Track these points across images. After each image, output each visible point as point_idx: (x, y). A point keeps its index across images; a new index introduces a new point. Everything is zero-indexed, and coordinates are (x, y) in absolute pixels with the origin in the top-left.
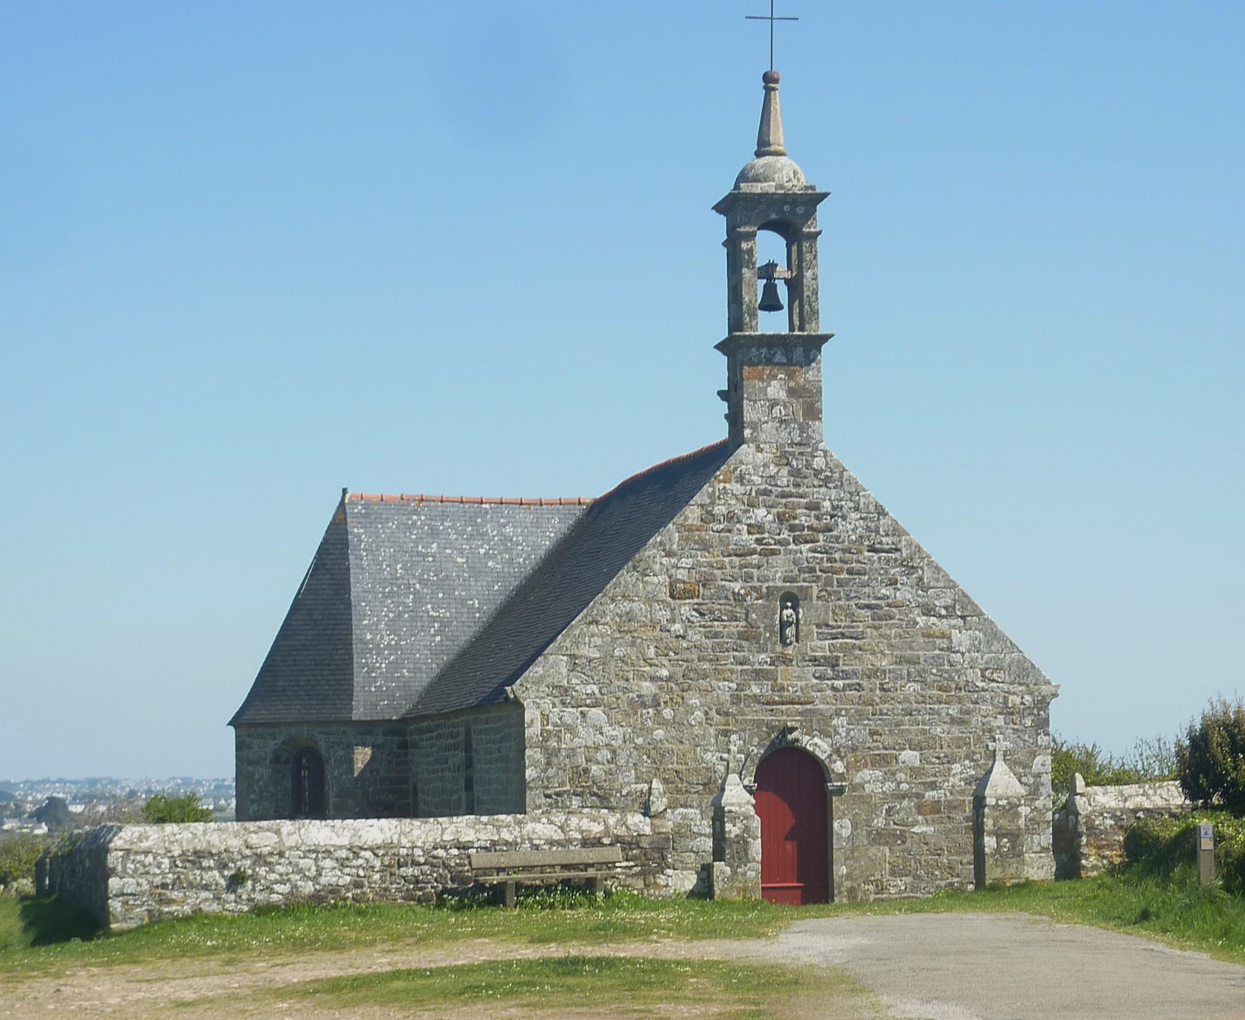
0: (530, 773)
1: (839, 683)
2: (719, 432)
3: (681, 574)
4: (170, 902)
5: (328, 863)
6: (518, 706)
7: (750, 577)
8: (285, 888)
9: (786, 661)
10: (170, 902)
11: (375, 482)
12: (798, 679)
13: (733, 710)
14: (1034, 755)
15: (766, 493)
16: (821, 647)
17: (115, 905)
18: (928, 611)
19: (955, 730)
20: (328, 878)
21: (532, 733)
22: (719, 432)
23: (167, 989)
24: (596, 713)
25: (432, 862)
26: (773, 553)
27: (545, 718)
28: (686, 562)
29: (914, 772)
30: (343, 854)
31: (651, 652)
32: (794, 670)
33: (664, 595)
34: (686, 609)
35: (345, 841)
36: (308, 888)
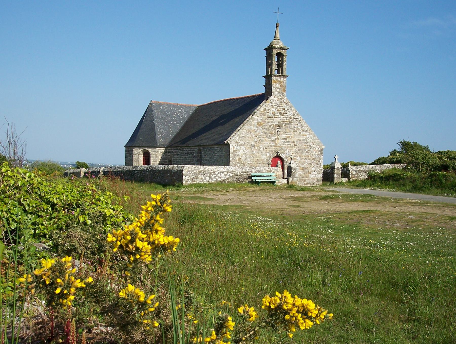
0: (231, 159)
1: (287, 144)
2: (263, 91)
3: (260, 121)
4: (194, 181)
5: (223, 175)
6: (228, 145)
7: (272, 122)
8: (215, 179)
9: (278, 139)
10: (194, 181)
11: (157, 99)
12: (280, 142)
13: (268, 148)
14: (320, 159)
15: (276, 106)
16: (284, 136)
17: (184, 182)
18: (303, 131)
19: (307, 154)
20: (223, 178)
21: (231, 151)
22: (263, 91)
23: (398, 209)
24: (243, 147)
25: (241, 175)
26: (276, 117)
27: (234, 148)
28: (261, 118)
29: (300, 162)
30: (225, 173)
31: (254, 136)
32: (280, 140)
33: (256, 125)
34: (260, 128)
35: (225, 170)
36: (219, 179)
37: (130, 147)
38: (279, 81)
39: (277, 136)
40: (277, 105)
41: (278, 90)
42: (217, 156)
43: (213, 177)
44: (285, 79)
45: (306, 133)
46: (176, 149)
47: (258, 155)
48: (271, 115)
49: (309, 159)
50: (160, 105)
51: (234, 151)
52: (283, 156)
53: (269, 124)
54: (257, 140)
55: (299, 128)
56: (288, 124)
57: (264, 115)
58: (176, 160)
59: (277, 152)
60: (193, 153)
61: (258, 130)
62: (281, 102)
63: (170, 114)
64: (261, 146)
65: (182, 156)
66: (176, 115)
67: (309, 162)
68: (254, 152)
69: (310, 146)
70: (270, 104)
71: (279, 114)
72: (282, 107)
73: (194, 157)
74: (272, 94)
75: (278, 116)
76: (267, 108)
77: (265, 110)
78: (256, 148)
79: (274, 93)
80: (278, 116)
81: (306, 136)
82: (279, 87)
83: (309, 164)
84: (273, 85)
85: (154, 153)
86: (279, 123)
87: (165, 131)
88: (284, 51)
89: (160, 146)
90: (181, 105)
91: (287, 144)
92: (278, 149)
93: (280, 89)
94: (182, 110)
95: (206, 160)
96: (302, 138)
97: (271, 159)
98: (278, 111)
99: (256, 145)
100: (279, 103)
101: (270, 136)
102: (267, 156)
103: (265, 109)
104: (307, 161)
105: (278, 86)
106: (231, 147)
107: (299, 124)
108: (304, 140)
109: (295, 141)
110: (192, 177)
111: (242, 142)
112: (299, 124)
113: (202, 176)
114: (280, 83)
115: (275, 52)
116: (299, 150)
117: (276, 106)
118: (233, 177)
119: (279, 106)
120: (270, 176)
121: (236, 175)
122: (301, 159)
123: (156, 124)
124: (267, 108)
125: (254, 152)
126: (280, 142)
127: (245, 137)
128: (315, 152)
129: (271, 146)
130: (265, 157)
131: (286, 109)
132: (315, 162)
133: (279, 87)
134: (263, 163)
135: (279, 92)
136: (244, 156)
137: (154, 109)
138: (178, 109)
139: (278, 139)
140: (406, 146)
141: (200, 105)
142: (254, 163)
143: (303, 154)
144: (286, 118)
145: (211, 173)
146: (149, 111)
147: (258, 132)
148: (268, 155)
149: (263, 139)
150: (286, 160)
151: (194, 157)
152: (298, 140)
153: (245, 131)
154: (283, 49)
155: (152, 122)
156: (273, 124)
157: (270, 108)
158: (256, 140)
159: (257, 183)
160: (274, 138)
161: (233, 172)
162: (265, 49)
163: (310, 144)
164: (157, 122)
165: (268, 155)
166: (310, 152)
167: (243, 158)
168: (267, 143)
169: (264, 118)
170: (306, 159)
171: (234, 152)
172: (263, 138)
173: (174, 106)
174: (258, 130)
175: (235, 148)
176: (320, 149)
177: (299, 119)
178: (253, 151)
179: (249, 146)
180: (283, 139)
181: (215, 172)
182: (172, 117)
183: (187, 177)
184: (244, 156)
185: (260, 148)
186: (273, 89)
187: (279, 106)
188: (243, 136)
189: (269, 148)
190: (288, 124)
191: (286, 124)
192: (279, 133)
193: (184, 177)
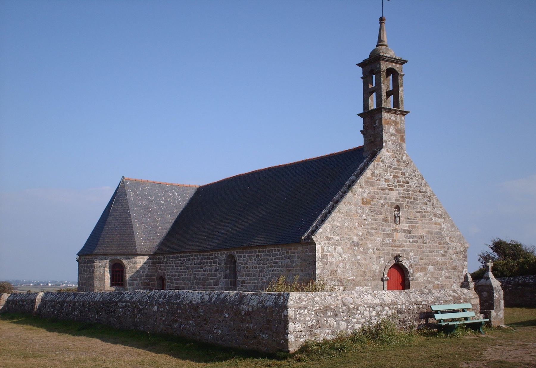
0: (318, 272)
1: (411, 240)
3: (365, 195)
7: (386, 198)
9: (397, 230)
11: (134, 174)
13: (381, 248)
14: (463, 268)
16: (405, 226)
18: (435, 215)
19: (443, 258)
21: (318, 255)
22: (357, 141)
24: (339, 248)
26: (392, 190)
28: (367, 191)
29: (432, 274)
30: (379, 308)
33: (360, 204)
34: (367, 208)
35: (378, 301)
37: (87, 255)
38: (394, 121)
39: (394, 225)
40: (393, 167)
41: (393, 138)
42: (279, 266)
43: (355, 320)
44: (403, 118)
45: (439, 220)
46: (174, 257)
47: (364, 262)
48: (384, 185)
49: (447, 269)
50: (138, 183)
51: (323, 256)
52: (406, 263)
53: (382, 201)
54: (363, 234)
55: (429, 209)
56: (412, 203)
57: (372, 184)
58: (175, 276)
59: (397, 257)
60: (215, 262)
61: (363, 213)
62: (398, 161)
63: (156, 198)
64: (370, 246)
65: (188, 268)
66: (166, 201)
67: (447, 275)
68: (359, 257)
69: (447, 244)
70: (381, 164)
71: (396, 183)
72: (401, 170)
73: (216, 271)
74: (384, 144)
75: (395, 186)
76: (377, 172)
77: (373, 174)
78: (362, 249)
79: (386, 142)
80: (395, 186)
81: (440, 224)
82: (394, 132)
83: (447, 278)
84: (384, 128)
85: (132, 265)
86: (397, 200)
87: (149, 230)
88: (398, 66)
89: (143, 253)
90: (172, 185)
91: (411, 240)
92: (398, 251)
93: (395, 135)
94: (173, 193)
95: (248, 275)
96: (435, 229)
97: (387, 271)
98: (395, 177)
99: (360, 242)
100: (395, 163)
101: (383, 225)
102: (380, 265)
103: (374, 173)
104: (443, 272)
105: (392, 130)
106: (318, 247)
107: (428, 203)
108: (437, 233)
109: (424, 234)
110: (310, 323)
111: (337, 238)
112: (428, 203)
113: (331, 321)
114: (396, 125)
115: (384, 66)
116: (430, 252)
117: (390, 167)
118: (393, 316)
119: (396, 169)
120: (463, 310)
121: (400, 312)
122: (435, 269)
123: (133, 215)
124: (377, 172)
125: (359, 257)
126: (400, 237)
127: (341, 227)
128: (454, 256)
129: (387, 245)
130: (376, 267)
131: (407, 175)
132: (456, 273)
133: (394, 132)
134: (374, 279)
135: (394, 141)
136: (341, 265)
137: (129, 191)
138: (167, 191)
139: (397, 230)
140: (498, 246)
141: (201, 185)
142: (359, 278)
143: (438, 259)
144: (408, 191)
145: (349, 310)
146: (119, 195)
147: (364, 216)
148: (382, 262)
149: (373, 231)
150: (411, 271)
151: (216, 271)
152: (429, 232)
153: (341, 215)
154: (396, 63)
155: (126, 211)
156: (388, 203)
157: (381, 171)
158: (360, 233)
159: (448, 329)
160: (390, 229)
161: (393, 303)
162: (359, 65)
163: (448, 239)
164: (134, 212)
165: (382, 262)
166: (448, 255)
167: (339, 271)
168: (379, 240)
169: (372, 189)
170: (442, 269)
171: (322, 258)
172: (372, 228)
173: (161, 186)
174: (363, 213)
175: (325, 250)
176: (462, 249)
177: (428, 194)
178: (356, 256)
179: (348, 246)
180: (405, 231)
181: (357, 309)
182: (158, 204)
183: (298, 326)
184: (341, 265)
185: (368, 249)
186: (385, 137)
187: (396, 169)
188: (339, 225)
189: (384, 250)
190: (412, 203)
191: (408, 202)
192: (397, 219)
193: (291, 326)
